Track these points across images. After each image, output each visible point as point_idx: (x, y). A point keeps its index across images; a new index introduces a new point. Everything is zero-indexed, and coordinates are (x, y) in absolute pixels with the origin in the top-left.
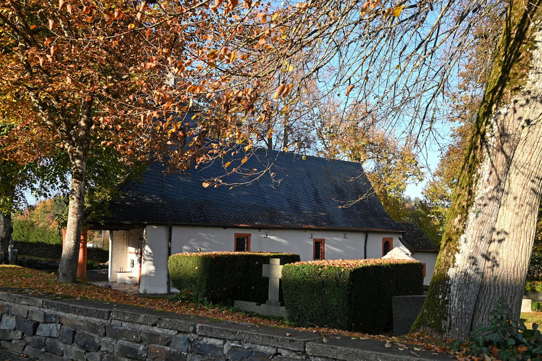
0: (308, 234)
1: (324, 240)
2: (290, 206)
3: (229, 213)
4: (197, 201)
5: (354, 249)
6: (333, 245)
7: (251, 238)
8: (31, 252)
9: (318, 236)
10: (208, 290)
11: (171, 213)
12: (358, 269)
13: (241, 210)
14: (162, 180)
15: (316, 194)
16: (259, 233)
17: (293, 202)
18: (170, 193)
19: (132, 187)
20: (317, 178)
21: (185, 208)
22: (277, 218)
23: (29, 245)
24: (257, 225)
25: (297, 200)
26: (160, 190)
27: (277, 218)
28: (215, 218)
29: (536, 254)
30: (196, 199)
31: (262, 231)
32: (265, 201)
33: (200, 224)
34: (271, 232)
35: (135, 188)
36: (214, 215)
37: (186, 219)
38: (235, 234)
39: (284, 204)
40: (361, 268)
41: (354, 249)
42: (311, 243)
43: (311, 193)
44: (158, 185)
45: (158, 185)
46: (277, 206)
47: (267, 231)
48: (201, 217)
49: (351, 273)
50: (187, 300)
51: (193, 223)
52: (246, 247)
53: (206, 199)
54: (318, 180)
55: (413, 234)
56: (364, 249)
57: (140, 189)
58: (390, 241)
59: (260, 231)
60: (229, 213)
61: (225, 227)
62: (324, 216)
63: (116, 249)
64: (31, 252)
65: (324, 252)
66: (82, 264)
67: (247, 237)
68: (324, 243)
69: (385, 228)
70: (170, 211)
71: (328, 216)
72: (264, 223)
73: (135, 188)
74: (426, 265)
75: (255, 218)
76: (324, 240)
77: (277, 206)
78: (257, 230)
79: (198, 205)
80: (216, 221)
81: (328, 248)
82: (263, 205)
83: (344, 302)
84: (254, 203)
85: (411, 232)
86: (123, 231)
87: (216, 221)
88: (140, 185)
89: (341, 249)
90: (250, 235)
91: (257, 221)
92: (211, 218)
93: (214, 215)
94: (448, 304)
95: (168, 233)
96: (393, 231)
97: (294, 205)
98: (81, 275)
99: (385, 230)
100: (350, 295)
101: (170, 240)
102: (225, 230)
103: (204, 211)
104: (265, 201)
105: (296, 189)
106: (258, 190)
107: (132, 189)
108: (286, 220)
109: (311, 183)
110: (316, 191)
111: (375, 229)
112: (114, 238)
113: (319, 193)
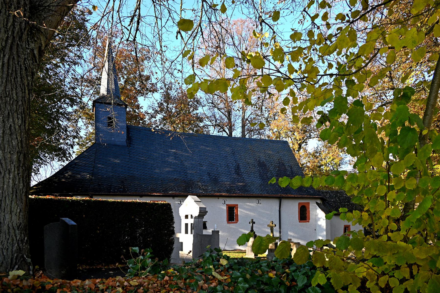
0: (221, 200)
1: (237, 205)
2: (209, 179)
5: (268, 212)
6: (246, 209)
9: (232, 202)
11: (95, 186)
15: (238, 168)
16: (173, 200)
17: (213, 175)
18: (99, 171)
20: (242, 155)
22: (192, 188)
25: (218, 173)
26: (92, 169)
31: (176, 198)
32: (186, 175)
33: (117, 193)
35: (72, 169)
38: (299, 204)
39: (204, 177)
41: (268, 212)
42: (225, 208)
43: (232, 167)
44: (90, 165)
47: (180, 198)
54: (242, 157)
55: (340, 200)
56: (278, 212)
58: (306, 205)
59: (218, 198)
62: (241, 185)
65: (237, 215)
68: (238, 208)
69: (301, 195)
71: (244, 186)
74: (226, 222)
76: (237, 205)
78: (171, 198)
81: (241, 212)
82: (183, 178)
84: (175, 177)
85: (339, 198)
89: (254, 213)
96: (309, 196)
97: (214, 177)
99: (300, 196)
102: (141, 198)
104: (186, 175)
105: (218, 164)
106: (181, 166)
108: (200, 189)
109: (234, 159)
110: (239, 165)
111: (289, 195)
113: (241, 167)
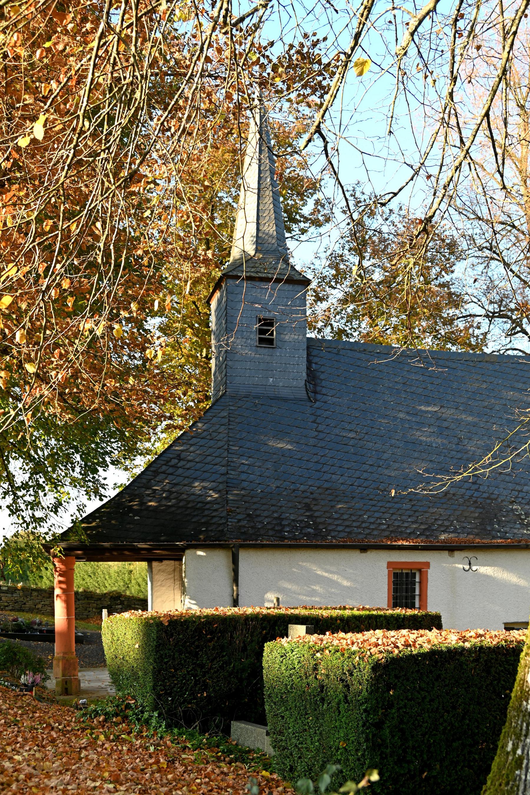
3: (377, 515)
4: (303, 492)
7: (429, 571)
8: (40, 606)
10: (159, 696)
11: (239, 520)
12: (412, 657)
13: (409, 506)
14: (228, 450)
16: (450, 559)
18: (243, 476)
19: (164, 468)
21: (273, 508)
22: (499, 522)
23: (35, 594)
24: (444, 541)
26: (223, 470)
27: (499, 522)
28: (340, 528)
29: (339, 621)
30: (302, 488)
31: (457, 554)
33: (302, 542)
34: (481, 556)
35: (171, 470)
36: (339, 522)
37: (271, 533)
38: (390, 564)
40: (424, 655)
44: (218, 460)
45: (218, 460)
46: (505, 493)
47: (470, 554)
48: (308, 526)
49: (376, 667)
50: (116, 715)
51: (286, 542)
52: (417, 592)
53: (326, 485)
57: (180, 471)
59: (451, 556)
60: (377, 515)
61: (364, 549)
63: (159, 600)
64: (40, 606)
66: (66, 634)
67: (420, 571)
70: (239, 517)
72: (462, 536)
73: (171, 470)
75: (440, 526)
77: (505, 493)
78: (446, 553)
79: (307, 501)
80: (342, 535)
82: (469, 493)
83: (359, 743)
86: (172, 562)
87: (342, 535)
88: (182, 463)
90: (427, 565)
91: (444, 531)
92: (330, 528)
93: (339, 522)
94: (521, 768)
95: (231, 566)
98: (65, 653)
100: (379, 725)
101: (236, 580)
102: (364, 555)
103: (316, 514)
107: (164, 473)
112: (156, 577)
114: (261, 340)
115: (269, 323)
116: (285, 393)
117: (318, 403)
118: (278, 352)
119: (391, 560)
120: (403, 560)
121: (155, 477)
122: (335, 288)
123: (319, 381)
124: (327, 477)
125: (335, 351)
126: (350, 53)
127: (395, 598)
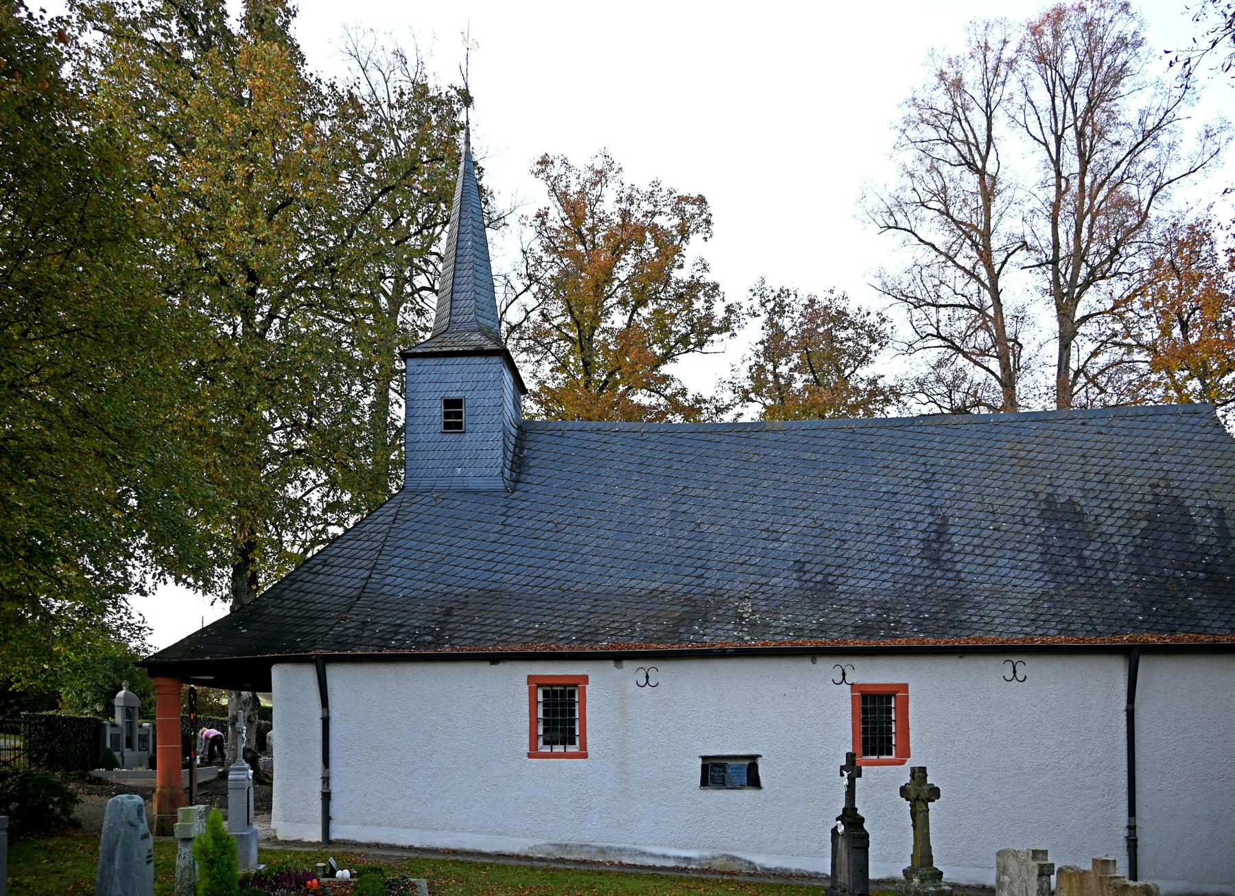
61: (495, 659)
90: (585, 679)
102: (495, 667)
107: (302, 581)
114: (447, 426)
115: (458, 403)
116: (475, 484)
117: (516, 493)
118: (467, 437)
119: (533, 674)
120: (556, 673)
121: (291, 585)
122: (753, 401)
123: (526, 468)
124: (497, 577)
125: (560, 433)
126: (977, 220)
127: (865, 741)
